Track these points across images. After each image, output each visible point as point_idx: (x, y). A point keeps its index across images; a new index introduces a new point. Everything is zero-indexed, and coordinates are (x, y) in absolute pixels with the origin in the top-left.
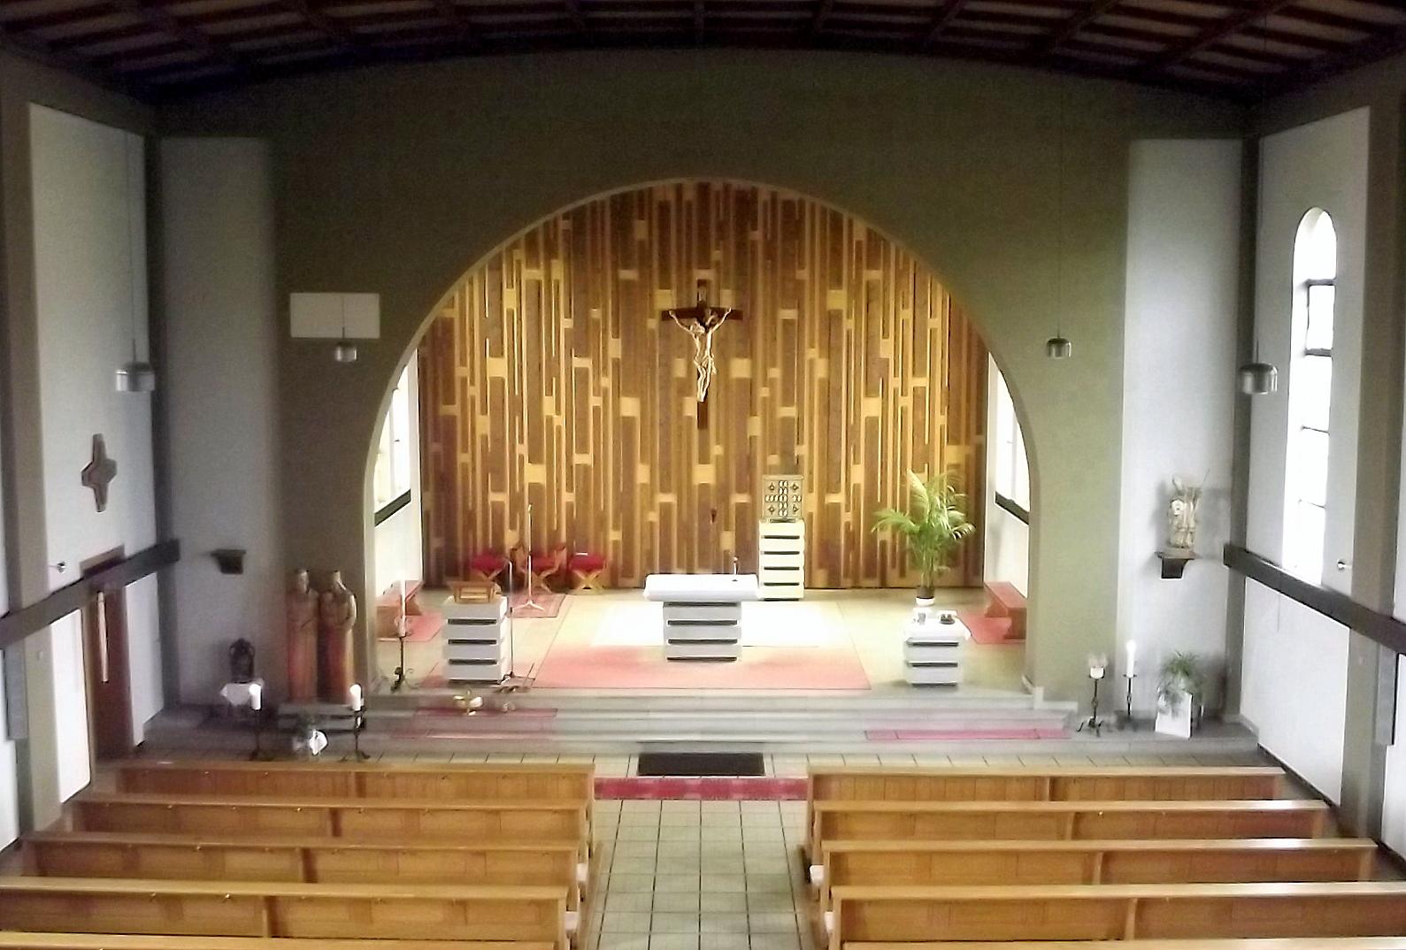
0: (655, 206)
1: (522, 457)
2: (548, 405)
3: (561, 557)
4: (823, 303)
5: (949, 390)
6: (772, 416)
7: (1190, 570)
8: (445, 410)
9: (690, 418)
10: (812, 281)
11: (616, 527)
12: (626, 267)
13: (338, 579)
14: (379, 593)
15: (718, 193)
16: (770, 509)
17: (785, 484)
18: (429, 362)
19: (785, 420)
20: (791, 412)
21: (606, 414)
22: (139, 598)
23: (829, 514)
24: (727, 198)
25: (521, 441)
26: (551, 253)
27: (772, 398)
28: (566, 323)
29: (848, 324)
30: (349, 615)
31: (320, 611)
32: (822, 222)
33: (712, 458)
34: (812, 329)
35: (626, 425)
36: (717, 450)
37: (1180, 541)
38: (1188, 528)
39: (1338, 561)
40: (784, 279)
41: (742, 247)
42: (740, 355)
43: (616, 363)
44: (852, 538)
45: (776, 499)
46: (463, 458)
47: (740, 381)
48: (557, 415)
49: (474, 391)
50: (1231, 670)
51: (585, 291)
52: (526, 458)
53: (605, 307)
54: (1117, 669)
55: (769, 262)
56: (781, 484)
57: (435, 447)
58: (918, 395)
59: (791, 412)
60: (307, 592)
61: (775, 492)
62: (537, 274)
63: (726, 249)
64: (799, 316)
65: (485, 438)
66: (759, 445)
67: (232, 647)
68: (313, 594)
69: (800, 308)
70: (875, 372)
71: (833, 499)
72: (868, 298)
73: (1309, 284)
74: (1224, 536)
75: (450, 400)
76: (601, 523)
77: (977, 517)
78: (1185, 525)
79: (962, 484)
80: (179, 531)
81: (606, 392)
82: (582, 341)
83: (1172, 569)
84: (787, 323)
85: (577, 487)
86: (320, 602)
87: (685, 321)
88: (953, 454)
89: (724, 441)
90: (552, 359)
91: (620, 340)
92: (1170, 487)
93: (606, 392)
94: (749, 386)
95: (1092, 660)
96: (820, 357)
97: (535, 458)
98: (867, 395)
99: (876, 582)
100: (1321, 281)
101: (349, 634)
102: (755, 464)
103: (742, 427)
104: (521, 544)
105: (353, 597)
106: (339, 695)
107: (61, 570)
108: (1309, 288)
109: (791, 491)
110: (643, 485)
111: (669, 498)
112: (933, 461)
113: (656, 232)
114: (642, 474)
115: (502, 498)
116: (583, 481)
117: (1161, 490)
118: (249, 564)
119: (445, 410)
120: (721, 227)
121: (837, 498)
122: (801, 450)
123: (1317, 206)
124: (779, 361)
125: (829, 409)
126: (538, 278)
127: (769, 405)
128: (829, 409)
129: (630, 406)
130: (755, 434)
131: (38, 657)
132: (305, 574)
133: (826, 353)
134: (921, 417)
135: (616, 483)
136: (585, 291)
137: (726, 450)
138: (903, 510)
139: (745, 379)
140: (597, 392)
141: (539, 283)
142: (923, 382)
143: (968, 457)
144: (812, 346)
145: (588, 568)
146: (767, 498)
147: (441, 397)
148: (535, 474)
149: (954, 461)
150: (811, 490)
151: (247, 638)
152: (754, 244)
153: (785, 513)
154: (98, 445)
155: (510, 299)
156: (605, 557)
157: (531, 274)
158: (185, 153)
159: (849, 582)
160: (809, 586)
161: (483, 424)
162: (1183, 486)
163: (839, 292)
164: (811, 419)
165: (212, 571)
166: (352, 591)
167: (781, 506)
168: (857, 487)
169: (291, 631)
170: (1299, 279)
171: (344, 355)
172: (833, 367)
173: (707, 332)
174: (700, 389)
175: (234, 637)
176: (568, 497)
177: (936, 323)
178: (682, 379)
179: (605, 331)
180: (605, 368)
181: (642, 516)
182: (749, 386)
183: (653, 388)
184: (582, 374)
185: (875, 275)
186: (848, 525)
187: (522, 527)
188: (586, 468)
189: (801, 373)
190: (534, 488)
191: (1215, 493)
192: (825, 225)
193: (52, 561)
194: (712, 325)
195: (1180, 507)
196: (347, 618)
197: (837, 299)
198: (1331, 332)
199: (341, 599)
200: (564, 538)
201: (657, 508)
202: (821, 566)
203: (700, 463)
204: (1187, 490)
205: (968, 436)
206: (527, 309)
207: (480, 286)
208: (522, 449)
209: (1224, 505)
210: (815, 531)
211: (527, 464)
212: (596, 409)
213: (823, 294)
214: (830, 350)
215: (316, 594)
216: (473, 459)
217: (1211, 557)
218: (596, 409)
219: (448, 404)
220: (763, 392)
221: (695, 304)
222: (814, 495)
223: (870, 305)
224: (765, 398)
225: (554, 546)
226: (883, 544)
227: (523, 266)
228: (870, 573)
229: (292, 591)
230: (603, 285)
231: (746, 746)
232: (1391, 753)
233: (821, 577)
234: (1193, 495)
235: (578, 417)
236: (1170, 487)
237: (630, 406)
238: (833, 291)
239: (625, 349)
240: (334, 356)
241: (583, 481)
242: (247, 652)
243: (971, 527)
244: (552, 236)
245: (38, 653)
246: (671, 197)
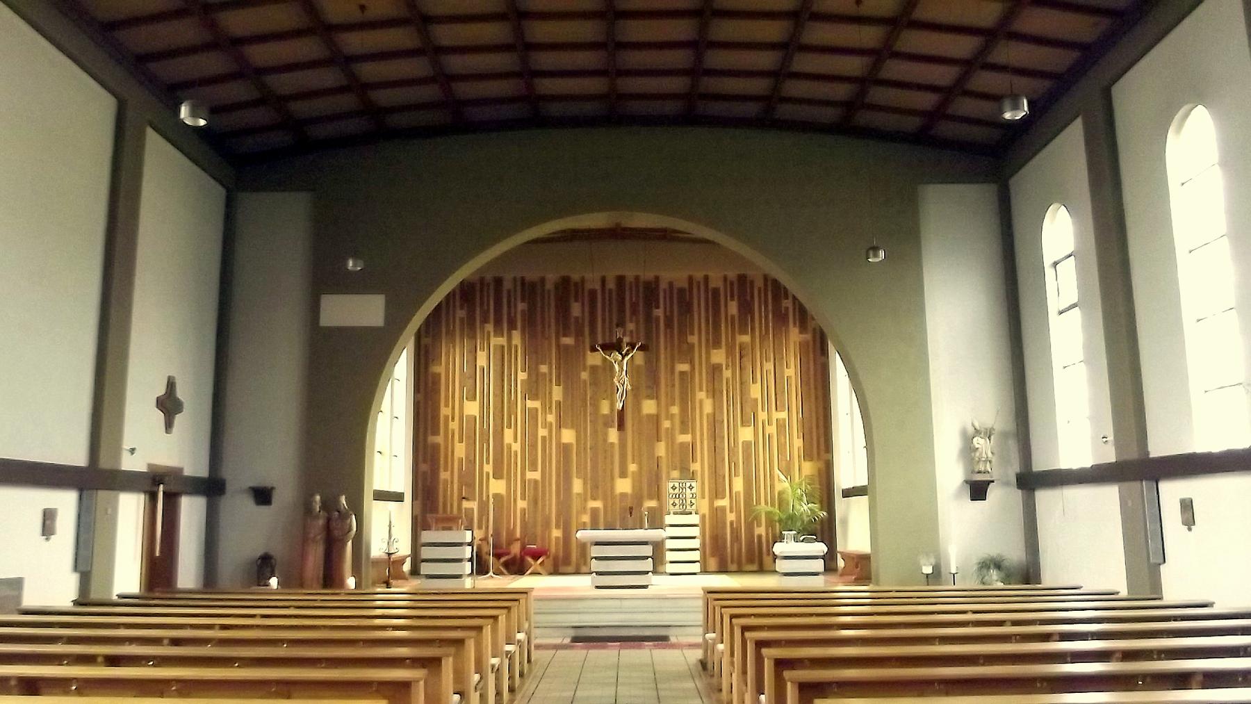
0: (586, 294)
1: (488, 474)
2: (508, 434)
3: (516, 549)
4: (708, 358)
5: (803, 423)
7: (993, 493)
8: (432, 439)
9: (612, 444)
11: (557, 527)
12: (565, 335)
13: (343, 500)
16: (673, 504)
17: (684, 485)
18: (422, 405)
19: (682, 444)
20: (687, 438)
22: (191, 510)
24: (637, 286)
25: (488, 462)
26: (512, 326)
27: (673, 428)
28: (522, 376)
29: (727, 374)
30: (350, 529)
31: (328, 528)
32: (705, 291)
33: (630, 473)
34: (701, 377)
35: (565, 449)
36: (632, 467)
38: (987, 457)
39: (1102, 436)
41: (649, 318)
42: (649, 397)
43: (559, 403)
46: (444, 475)
47: (649, 416)
49: (454, 425)
50: (1031, 570)
51: (536, 353)
53: (550, 364)
54: (943, 570)
55: (668, 330)
56: (681, 485)
57: (424, 467)
58: (780, 425)
59: (687, 438)
60: (320, 511)
62: (502, 341)
63: (637, 323)
65: (461, 460)
69: (692, 363)
70: (748, 409)
71: (720, 503)
72: (740, 356)
73: (1055, 264)
74: (1015, 468)
75: (436, 432)
76: (547, 525)
77: (829, 505)
78: (984, 455)
79: (817, 494)
80: (227, 473)
83: (978, 491)
84: (682, 373)
85: (528, 496)
86: (329, 520)
87: (608, 353)
88: (808, 468)
89: (638, 459)
90: (512, 402)
93: (551, 424)
94: (656, 420)
95: (923, 561)
96: (707, 397)
97: (498, 475)
98: (743, 425)
100: (1070, 307)
101: (350, 544)
102: (662, 476)
103: (652, 449)
104: (485, 539)
105: (354, 516)
106: (341, 584)
107: (132, 454)
108: (1055, 267)
109: (688, 490)
110: (578, 494)
111: (598, 504)
112: (794, 474)
113: (587, 309)
114: (577, 486)
116: (535, 493)
117: (964, 433)
121: (724, 503)
122: (696, 467)
124: (677, 401)
125: (714, 436)
128: (714, 436)
129: (568, 436)
130: (660, 455)
131: (106, 513)
132: (318, 498)
133: (711, 394)
134: (783, 440)
136: (536, 353)
137: (640, 468)
138: (773, 505)
139: (653, 415)
140: (544, 426)
142: (783, 415)
143: (819, 470)
144: (701, 390)
145: (536, 556)
147: (429, 431)
148: (497, 487)
151: (272, 553)
152: (658, 319)
153: (684, 507)
154: (171, 385)
155: (482, 360)
159: (734, 567)
160: (703, 562)
161: (460, 450)
162: (980, 427)
163: (720, 350)
164: (702, 442)
165: (248, 504)
166: (353, 511)
167: (681, 501)
168: (738, 493)
169: (305, 540)
170: (1048, 262)
171: (355, 265)
172: (717, 407)
173: (623, 358)
174: (619, 401)
175: (260, 553)
176: (522, 504)
177: (791, 371)
178: (606, 415)
179: (551, 381)
182: (656, 420)
183: (585, 421)
185: (746, 339)
186: (732, 523)
187: (487, 528)
188: (536, 482)
189: (693, 409)
190: (497, 497)
191: (1004, 435)
192: (708, 323)
193: (127, 444)
194: (627, 354)
195: (979, 442)
197: (719, 356)
198: (1077, 291)
199: (344, 516)
200: (518, 535)
201: (589, 511)
202: (713, 555)
203: (620, 477)
204: (983, 429)
205: (818, 454)
207: (460, 351)
208: (488, 468)
209: (1013, 446)
210: (707, 530)
211: (492, 480)
213: (708, 353)
214: (714, 393)
215: (326, 514)
217: (1007, 484)
218: (544, 438)
219: (434, 435)
220: (666, 424)
225: (510, 542)
228: (751, 560)
231: (652, 629)
232: (1164, 569)
233: (713, 563)
234: (989, 434)
235: (530, 443)
236: (971, 430)
237: (568, 436)
238: (715, 351)
239: (566, 393)
240: (346, 264)
241: (535, 493)
243: (825, 513)
244: (513, 315)
245: (106, 510)
246: (598, 287)
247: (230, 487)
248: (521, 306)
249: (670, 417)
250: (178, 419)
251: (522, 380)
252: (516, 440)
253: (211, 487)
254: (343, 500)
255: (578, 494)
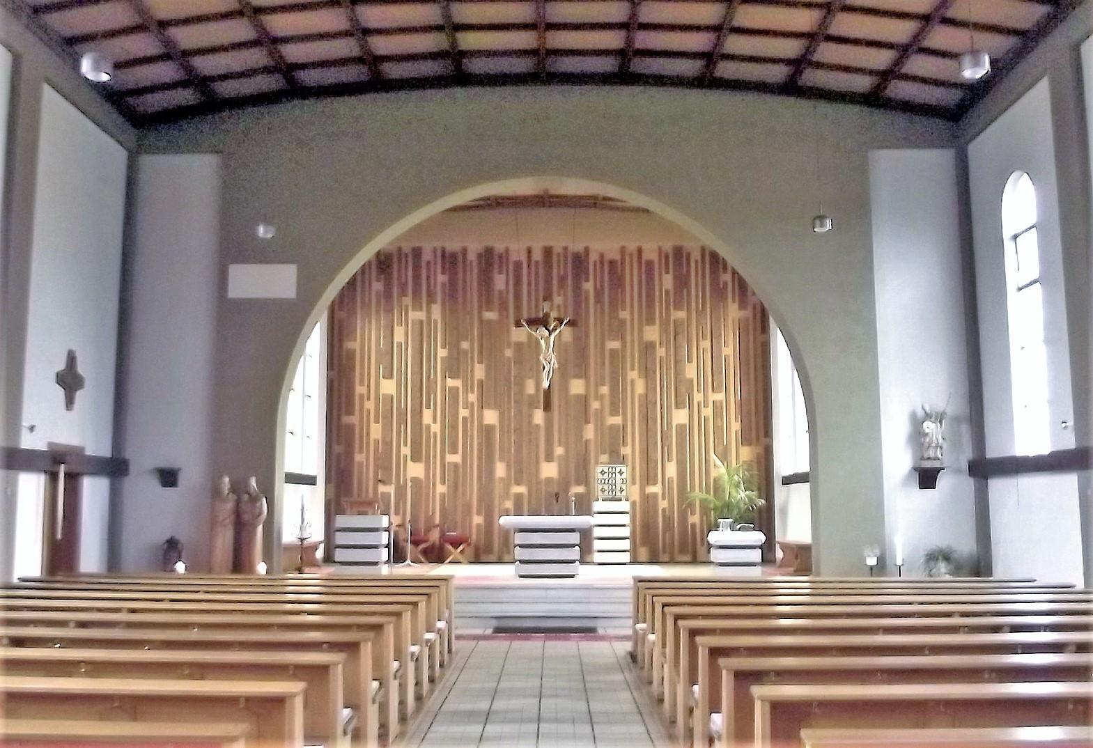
1: (405, 457)
5: (741, 405)
6: (602, 424)
7: (943, 481)
8: (346, 419)
9: (537, 426)
10: (632, 320)
11: (479, 513)
12: (489, 309)
13: (253, 482)
14: (267, 18)
15: (559, 255)
16: (601, 490)
17: (614, 469)
19: (612, 427)
20: (617, 420)
21: (472, 422)
22: (93, 491)
23: (648, 502)
25: (406, 445)
27: (602, 410)
28: (442, 353)
29: (661, 352)
30: (260, 514)
31: (238, 514)
34: (633, 354)
35: (488, 431)
36: (559, 451)
37: (931, 453)
40: (611, 318)
42: (577, 376)
44: (668, 520)
45: (606, 482)
46: (359, 458)
47: (578, 396)
48: (434, 423)
49: (370, 405)
52: (409, 458)
57: (338, 449)
59: (617, 420)
61: (606, 475)
64: (622, 346)
65: (377, 441)
66: (592, 448)
67: (164, 543)
68: (232, 497)
70: (683, 389)
71: (652, 489)
72: (675, 333)
74: (967, 454)
75: (350, 412)
80: (130, 453)
81: (472, 404)
82: (455, 366)
83: (927, 478)
86: (238, 502)
87: (534, 328)
88: (746, 453)
91: (484, 365)
92: (920, 413)
94: (584, 400)
95: (867, 552)
96: (640, 377)
97: (416, 457)
98: (677, 407)
99: (688, 558)
101: (260, 528)
103: (580, 431)
105: (264, 499)
109: (618, 475)
111: (522, 489)
114: (500, 470)
115: (390, 489)
116: (456, 477)
118: (182, 479)
119: (346, 419)
120: (562, 280)
121: (656, 489)
122: (626, 451)
123: (1019, 169)
124: (607, 379)
125: (647, 419)
126: (421, 318)
127: (600, 414)
128: (647, 419)
129: (491, 417)
132: (227, 480)
135: (480, 478)
140: (465, 407)
141: (421, 322)
142: (720, 397)
143: (758, 456)
145: (456, 543)
146: (599, 482)
148: (415, 470)
149: (745, 459)
150: (634, 483)
153: (614, 493)
154: (71, 359)
155: (399, 335)
156: (470, 537)
157: (416, 315)
158: (156, 165)
159: (666, 558)
160: (633, 551)
161: (376, 431)
165: (154, 484)
167: (610, 487)
168: (670, 480)
169: (213, 524)
172: (649, 386)
174: (545, 378)
175: (167, 536)
176: (441, 489)
177: (729, 350)
179: (472, 358)
180: (472, 387)
181: (500, 505)
182: (584, 400)
184: (454, 391)
185: (681, 315)
186: (664, 510)
188: (456, 465)
189: (624, 390)
190: (415, 481)
191: (957, 420)
194: (554, 330)
195: (929, 427)
196: (259, 516)
197: (652, 333)
199: (254, 500)
201: (512, 498)
205: (758, 439)
206: (412, 340)
208: (406, 451)
211: (410, 463)
212: (465, 419)
213: (641, 331)
214: (647, 372)
216: (367, 459)
218: (465, 419)
220: (595, 405)
221: (541, 315)
222: (637, 487)
223: (677, 337)
224: (596, 410)
226: (693, 526)
227: (410, 308)
228: (683, 550)
229: (216, 492)
230: (472, 325)
233: (643, 553)
234: (940, 418)
235: (451, 424)
236: (920, 413)
237: (491, 417)
242: (176, 548)
243: (763, 501)
246: (524, 258)
247: (133, 468)
248: (442, 278)
249: (600, 398)
250: (79, 395)
251: (442, 358)
252: (435, 421)
253: (115, 468)
254: (253, 482)
255: (501, 479)
